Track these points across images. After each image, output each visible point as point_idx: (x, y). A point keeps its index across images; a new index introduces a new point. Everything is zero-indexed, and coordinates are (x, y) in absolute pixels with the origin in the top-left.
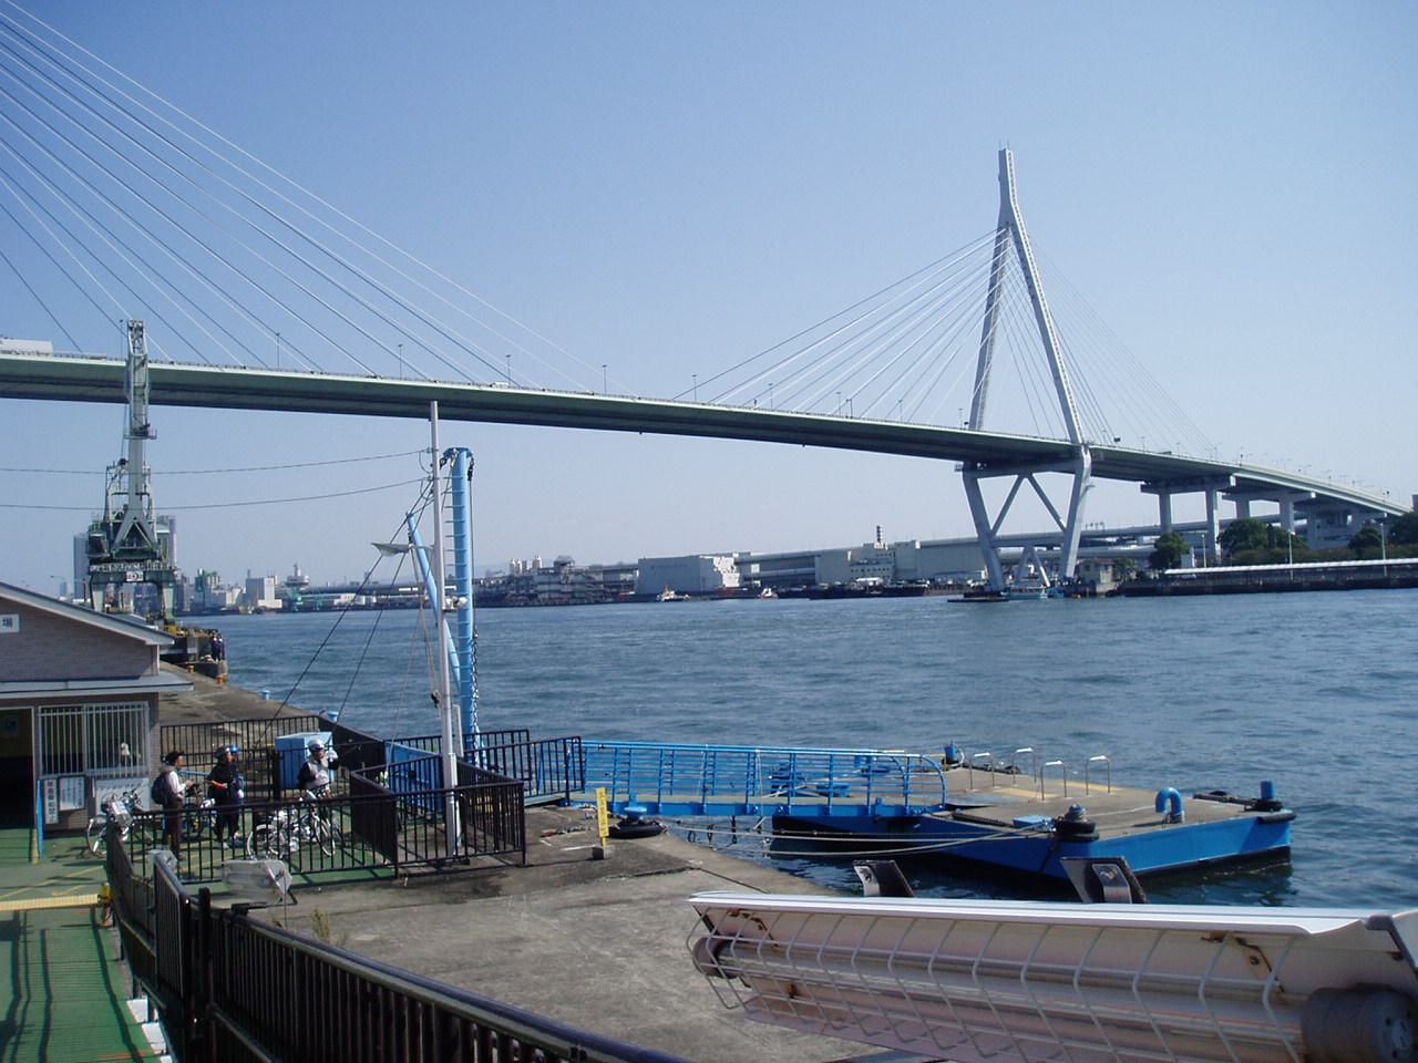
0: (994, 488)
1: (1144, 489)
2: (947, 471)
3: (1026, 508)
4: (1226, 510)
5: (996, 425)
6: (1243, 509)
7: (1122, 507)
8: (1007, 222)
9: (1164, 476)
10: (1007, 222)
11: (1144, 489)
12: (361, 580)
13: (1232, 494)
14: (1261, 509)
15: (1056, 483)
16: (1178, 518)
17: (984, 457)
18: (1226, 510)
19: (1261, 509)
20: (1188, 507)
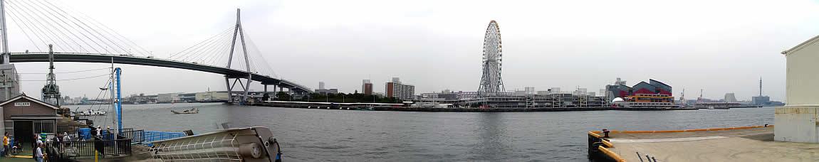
0: (232, 81)
1: (412, 88)
2: (222, 76)
3: (238, 85)
4: (278, 89)
5: (233, 67)
6: (281, 89)
7: (257, 87)
8: (238, 26)
9: (266, 81)
10: (238, 26)
11: (412, 88)
12: (723, 98)
13: (279, 86)
14: (285, 90)
15: (244, 81)
16: (268, 90)
17: (230, 74)
18: (278, 89)
19: (285, 90)
20: (270, 88)
